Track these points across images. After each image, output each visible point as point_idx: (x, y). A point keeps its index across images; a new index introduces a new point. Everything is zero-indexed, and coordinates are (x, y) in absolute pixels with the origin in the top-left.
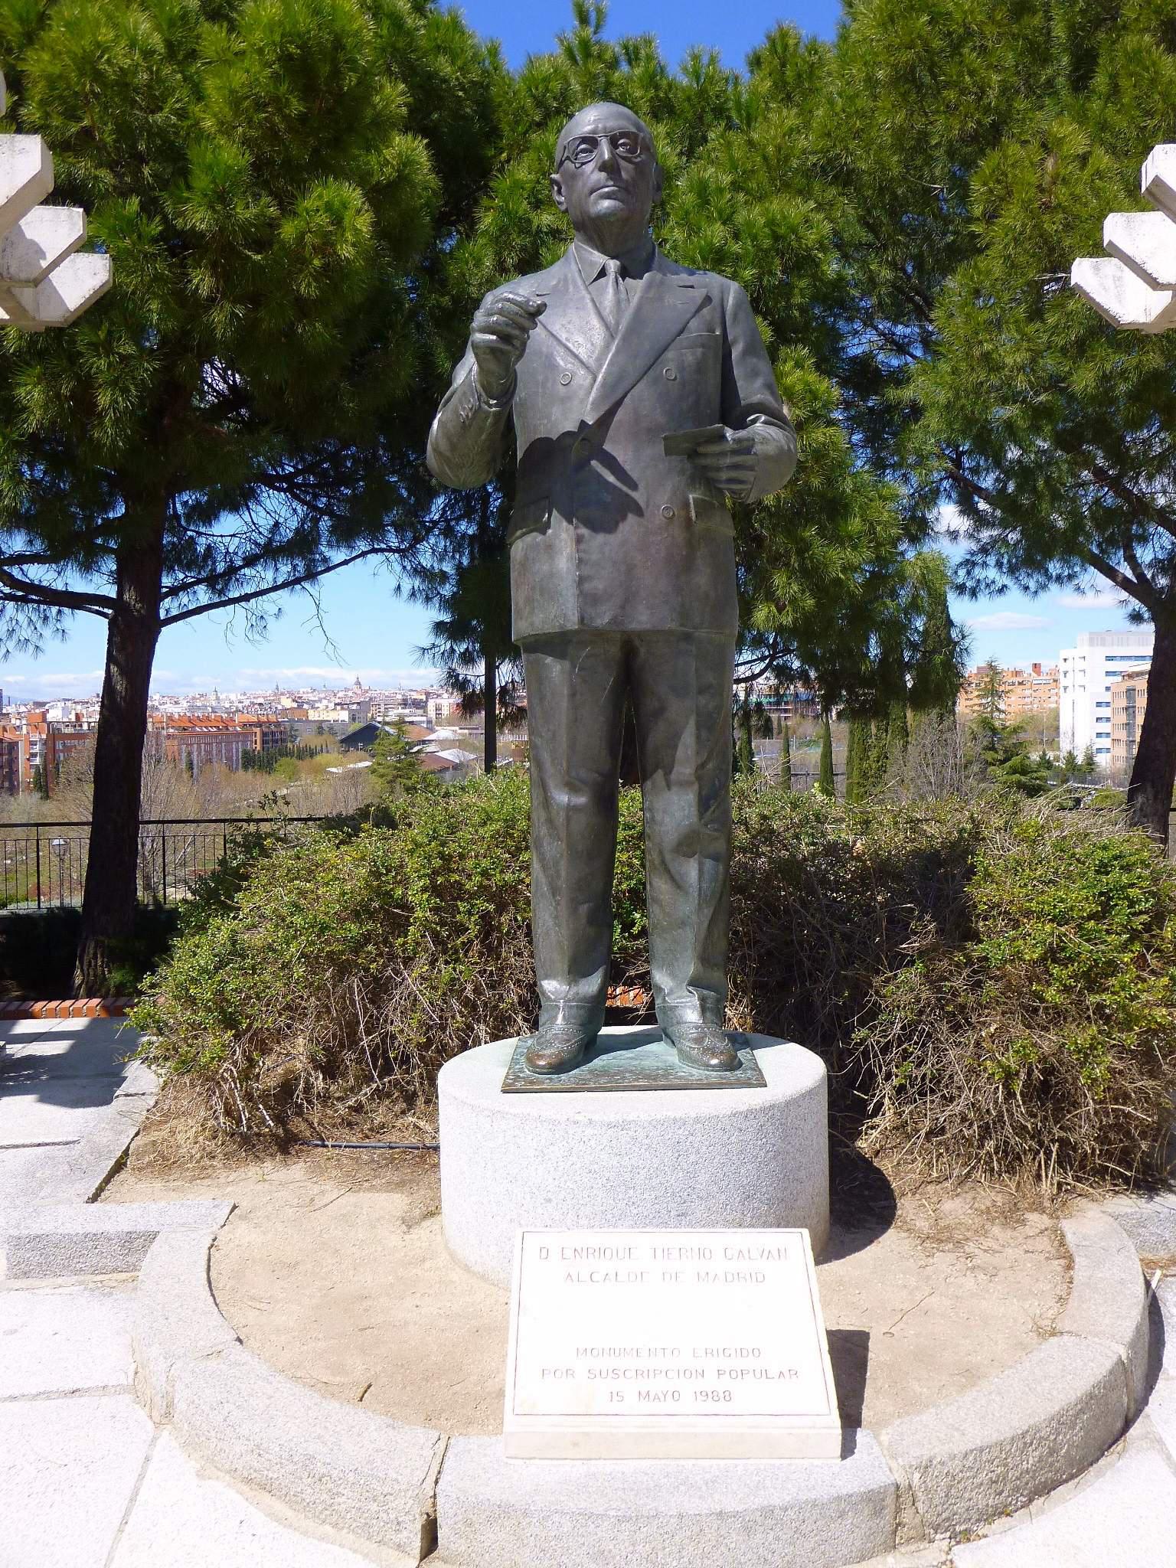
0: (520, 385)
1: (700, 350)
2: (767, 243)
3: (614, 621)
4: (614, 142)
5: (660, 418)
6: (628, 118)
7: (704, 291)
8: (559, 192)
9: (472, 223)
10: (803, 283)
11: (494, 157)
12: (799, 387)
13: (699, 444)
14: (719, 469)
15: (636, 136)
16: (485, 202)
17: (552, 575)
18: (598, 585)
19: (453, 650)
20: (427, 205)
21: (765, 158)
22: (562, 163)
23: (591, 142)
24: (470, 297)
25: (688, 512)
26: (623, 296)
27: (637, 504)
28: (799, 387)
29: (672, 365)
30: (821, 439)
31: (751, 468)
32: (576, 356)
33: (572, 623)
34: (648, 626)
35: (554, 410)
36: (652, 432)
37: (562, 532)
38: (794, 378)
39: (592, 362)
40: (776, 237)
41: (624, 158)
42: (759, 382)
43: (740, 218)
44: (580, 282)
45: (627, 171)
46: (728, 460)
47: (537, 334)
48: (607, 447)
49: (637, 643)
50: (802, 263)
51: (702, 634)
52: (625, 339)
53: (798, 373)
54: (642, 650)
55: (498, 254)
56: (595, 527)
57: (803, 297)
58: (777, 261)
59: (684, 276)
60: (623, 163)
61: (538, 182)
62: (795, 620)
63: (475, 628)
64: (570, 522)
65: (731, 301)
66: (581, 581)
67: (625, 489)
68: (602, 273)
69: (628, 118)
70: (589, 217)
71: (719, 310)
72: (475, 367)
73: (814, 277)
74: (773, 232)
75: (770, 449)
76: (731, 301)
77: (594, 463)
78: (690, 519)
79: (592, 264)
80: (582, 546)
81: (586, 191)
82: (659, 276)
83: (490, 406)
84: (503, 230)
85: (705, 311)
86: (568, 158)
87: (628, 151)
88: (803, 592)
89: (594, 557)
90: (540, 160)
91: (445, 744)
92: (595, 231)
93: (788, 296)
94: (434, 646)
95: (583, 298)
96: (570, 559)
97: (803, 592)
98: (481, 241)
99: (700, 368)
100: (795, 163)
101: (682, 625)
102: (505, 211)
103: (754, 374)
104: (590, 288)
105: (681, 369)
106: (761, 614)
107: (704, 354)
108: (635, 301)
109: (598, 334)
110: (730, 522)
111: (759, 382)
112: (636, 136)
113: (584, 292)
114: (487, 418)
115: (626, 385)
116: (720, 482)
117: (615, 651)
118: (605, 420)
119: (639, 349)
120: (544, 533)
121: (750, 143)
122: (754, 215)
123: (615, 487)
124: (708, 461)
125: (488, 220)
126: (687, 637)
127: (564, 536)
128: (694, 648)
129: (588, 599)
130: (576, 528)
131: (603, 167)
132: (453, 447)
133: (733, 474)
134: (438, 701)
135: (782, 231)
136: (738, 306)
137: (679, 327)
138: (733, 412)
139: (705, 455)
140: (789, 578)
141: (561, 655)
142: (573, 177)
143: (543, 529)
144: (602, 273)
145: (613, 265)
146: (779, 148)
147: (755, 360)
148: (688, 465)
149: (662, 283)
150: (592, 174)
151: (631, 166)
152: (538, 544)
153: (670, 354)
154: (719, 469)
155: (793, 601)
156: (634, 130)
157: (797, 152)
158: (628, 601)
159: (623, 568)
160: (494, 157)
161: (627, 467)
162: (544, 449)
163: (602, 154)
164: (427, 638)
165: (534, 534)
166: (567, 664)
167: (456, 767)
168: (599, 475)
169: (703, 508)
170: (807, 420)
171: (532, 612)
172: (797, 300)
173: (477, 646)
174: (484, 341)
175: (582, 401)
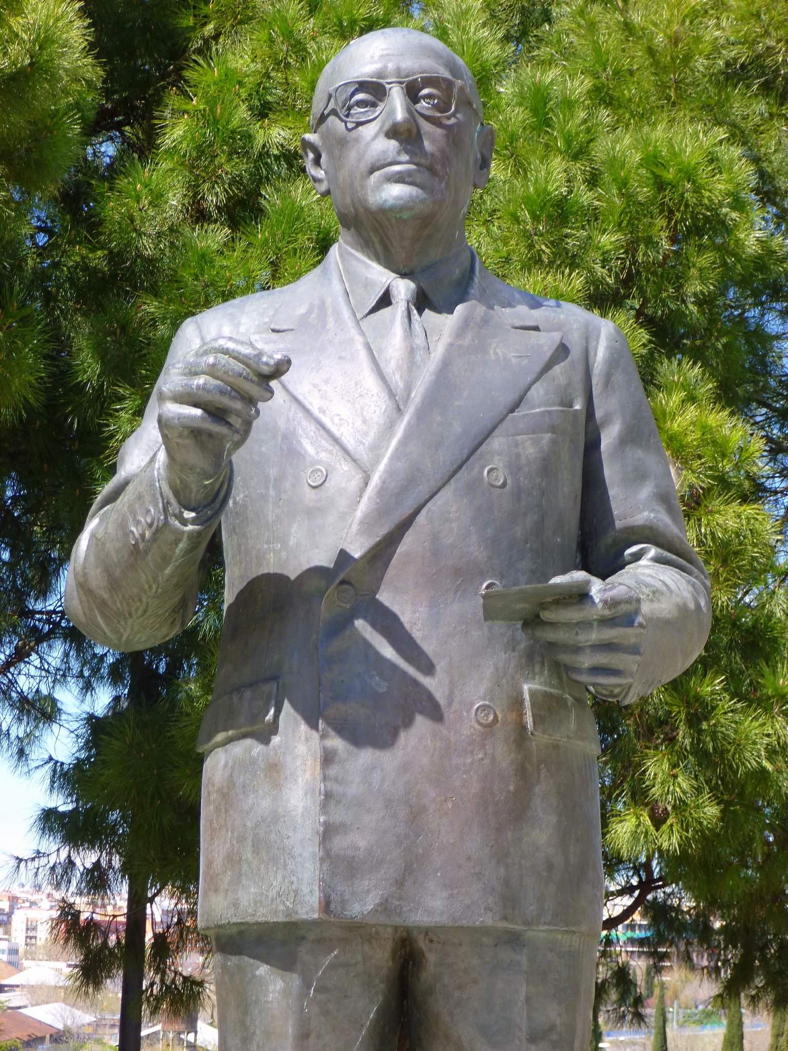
0: (237, 480)
1: (547, 437)
2: (644, 193)
3: (384, 907)
4: (412, 92)
5: (477, 552)
6: (436, 55)
7: (556, 336)
8: (317, 162)
9: (152, 135)
10: (705, 260)
11: (193, 29)
12: (693, 437)
13: (543, 606)
14: (577, 649)
15: (450, 84)
16: (173, 100)
17: (275, 818)
18: (358, 841)
19: (71, 863)
20: (77, 106)
21: (651, 51)
22: (323, 118)
23: (374, 90)
24: (139, 256)
25: (521, 715)
26: (419, 341)
27: (430, 697)
28: (693, 437)
29: (498, 462)
30: (732, 524)
31: (634, 650)
32: (336, 441)
33: (308, 907)
34: (443, 920)
35: (294, 528)
36: (464, 575)
37: (298, 743)
38: (686, 420)
39: (363, 454)
40: (660, 185)
41: (427, 118)
42: (646, 491)
43: (602, 148)
44: (346, 314)
45: (432, 139)
46: (595, 636)
47: (275, 409)
48: (384, 597)
49: (422, 944)
50: (705, 226)
51: (539, 933)
52: (422, 414)
53: (692, 412)
54: (431, 958)
55: (194, 189)
56: (358, 735)
57: (703, 280)
58: (660, 222)
59: (522, 309)
60: (426, 126)
61: (267, 76)
62: (684, 844)
63: (113, 828)
64: (314, 726)
65: (601, 354)
66: (328, 832)
67: (411, 670)
68: (385, 300)
69: (436, 55)
70: (367, 210)
71: (581, 368)
72: (162, 456)
73: (722, 249)
74: (657, 177)
75: (664, 608)
76: (601, 354)
77: (359, 623)
78: (523, 727)
79: (368, 284)
80: (333, 771)
81: (364, 166)
82: (481, 309)
83: (184, 522)
84: (202, 150)
85: (557, 369)
86: (334, 112)
87: (436, 107)
88: (699, 791)
89: (354, 788)
90: (271, 41)
91: (41, 995)
92: (376, 232)
93: (679, 281)
94: (39, 854)
95: (352, 340)
96: (310, 791)
97: (699, 791)
98: (165, 165)
99: (547, 466)
100: (700, 63)
101: (505, 918)
102: (210, 119)
103: (639, 476)
104: (364, 324)
105: (515, 468)
106: (625, 829)
107: (554, 442)
108: (439, 351)
109: (376, 405)
110: (593, 728)
111: (646, 491)
112: (450, 84)
113: (353, 332)
114: (177, 541)
115: (423, 490)
116: (578, 670)
117: (381, 957)
118: (382, 552)
119: (446, 443)
120: (266, 741)
121: (628, 27)
122: (622, 146)
123: (394, 667)
124: (559, 636)
125: (178, 132)
126: (513, 940)
127: (301, 749)
128: (524, 960)
129: (339, 866)
130: (323, 737)
131: (393, 132)
132: (114, 584)
133: (602, 659)
134: (33, 914)
135: (670, 175)
136: (613, 362)
137: (513, 396)
138: (599, 547)
139: (553, 625)
140: (674, 766)
141: (286, 964)
142: (342, 143)
143: (265, 735)
144: (385, 300)
145: (403, 289)
146: (675, 40)
147: (640, 453)
148: (520, 635)
149: (485, 321)
150: (373, 141)
151: (439, 131)
152: (253, 761)
153: (497, 443)
154: (577, 649)
155: (680, 807)
156: (447, 75)
157: (706, 47)
158: (409, 871)
159: (403, 812)
160: (193, 29)
161: (417, 634)
162: (273, 597)
163: (392, 112)
164: (27, 839)
165: (248, 742)
166: (295, 980)
167: (58, 1037)
168: (368, 645)
169: (548, 708)
170: (708, 490)
171: (237, 881)
172: (694, 287)
173: (117, 862)
174: (180, 417)
175: (343, 517)
